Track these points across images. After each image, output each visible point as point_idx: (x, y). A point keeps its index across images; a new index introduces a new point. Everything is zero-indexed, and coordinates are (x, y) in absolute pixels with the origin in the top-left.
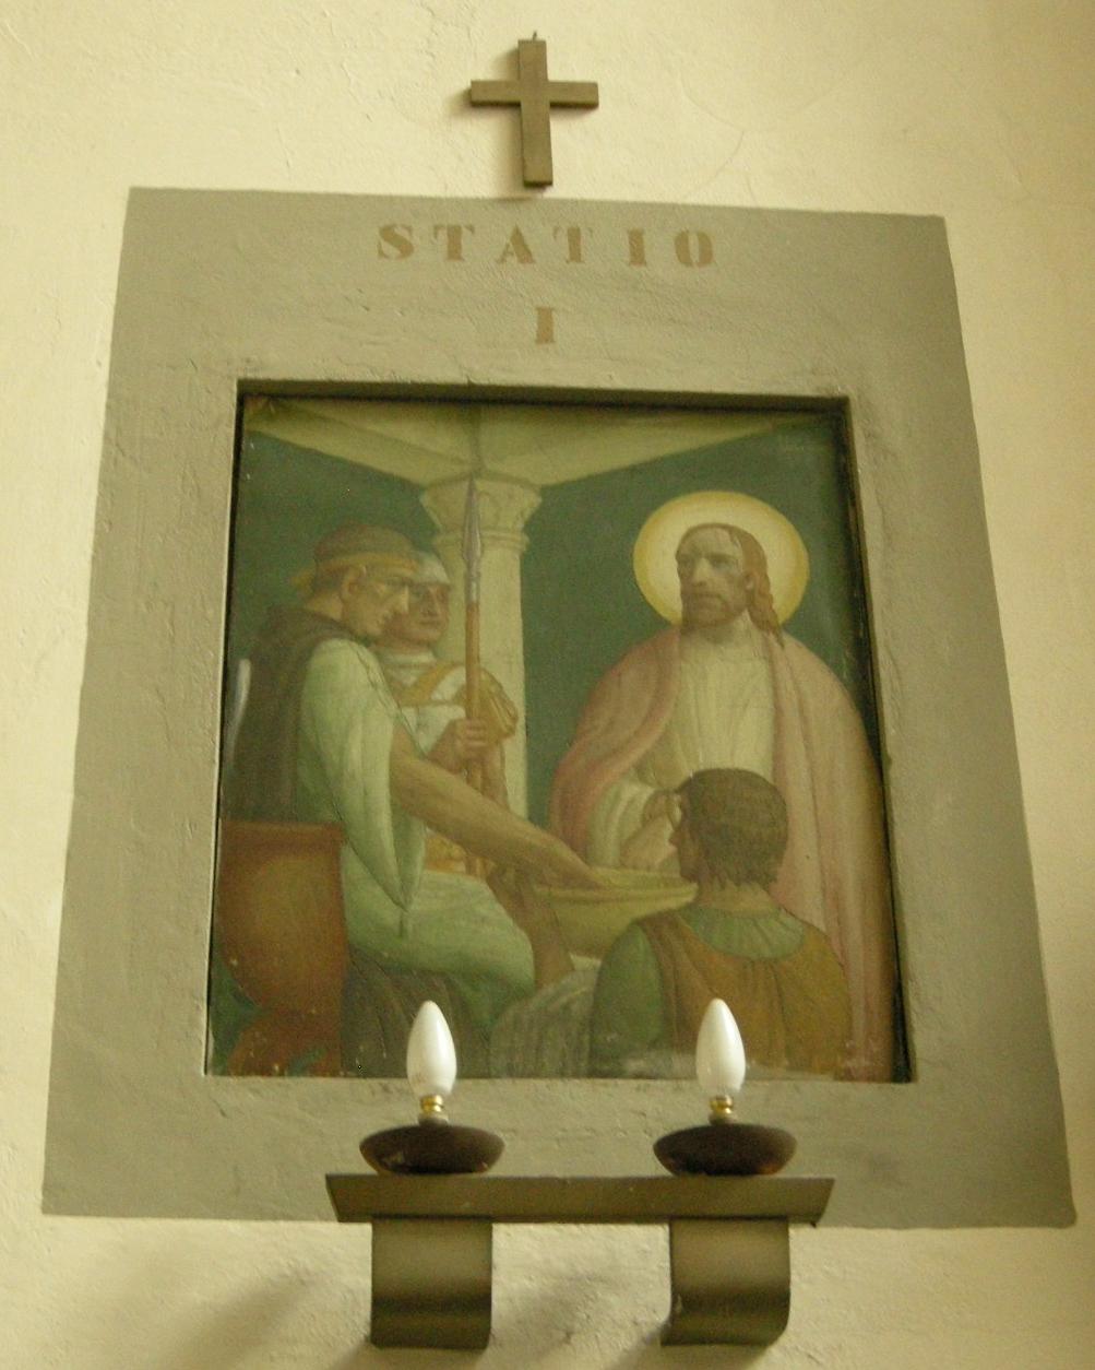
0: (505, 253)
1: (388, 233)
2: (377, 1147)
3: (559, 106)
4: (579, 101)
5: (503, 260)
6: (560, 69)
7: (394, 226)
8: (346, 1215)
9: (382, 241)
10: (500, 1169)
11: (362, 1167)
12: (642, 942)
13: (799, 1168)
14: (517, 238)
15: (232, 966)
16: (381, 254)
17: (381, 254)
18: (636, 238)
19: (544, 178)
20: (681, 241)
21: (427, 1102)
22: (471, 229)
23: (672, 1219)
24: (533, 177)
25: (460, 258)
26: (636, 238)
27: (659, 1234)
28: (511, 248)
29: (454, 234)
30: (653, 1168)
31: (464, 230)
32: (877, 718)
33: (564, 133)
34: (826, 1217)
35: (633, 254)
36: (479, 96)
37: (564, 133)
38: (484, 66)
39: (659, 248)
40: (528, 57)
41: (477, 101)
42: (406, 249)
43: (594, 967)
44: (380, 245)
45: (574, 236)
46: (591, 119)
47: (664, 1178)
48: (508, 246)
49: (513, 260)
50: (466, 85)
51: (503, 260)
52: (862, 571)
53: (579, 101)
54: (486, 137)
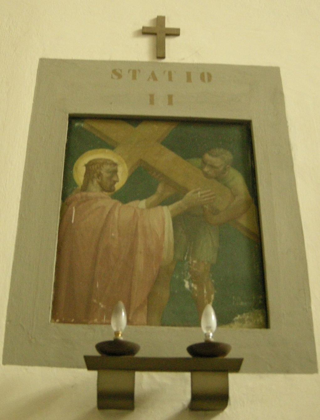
1: (114, 71)
2: (101, 347)
4: (175, 33)
5: (148, 80)
6: (169, 24)
8: (90, 368)
10: (139, 355)
11: (96, 353)
13: (231, 355)
14: (153, 74)
16: (121, 71)
17: (112, 78)
18: (189, 75)
20: (202, 75)
21: (117, 333)
22: (139, 71)
23: (192, 371)
24: (160, 56)
26: (189, 75)
27: (188, 375)
28: (151, 77)
29: (170, 74)
30: (187, 355)
32: (257, 191)
33: (170, 42)
36: (145, 31)
37: (170, 42)
38: (146, 21)
39: (195, 77)
40: (160, 20)
41: (145, 32)
42: (120, 76)
43: (210, 154)
45: (170, 74)
46: (177, 39)
49: (152, 80)
50: (141, 28)
51: (148, 80)
52: (256, 188)
53: (175, 33)
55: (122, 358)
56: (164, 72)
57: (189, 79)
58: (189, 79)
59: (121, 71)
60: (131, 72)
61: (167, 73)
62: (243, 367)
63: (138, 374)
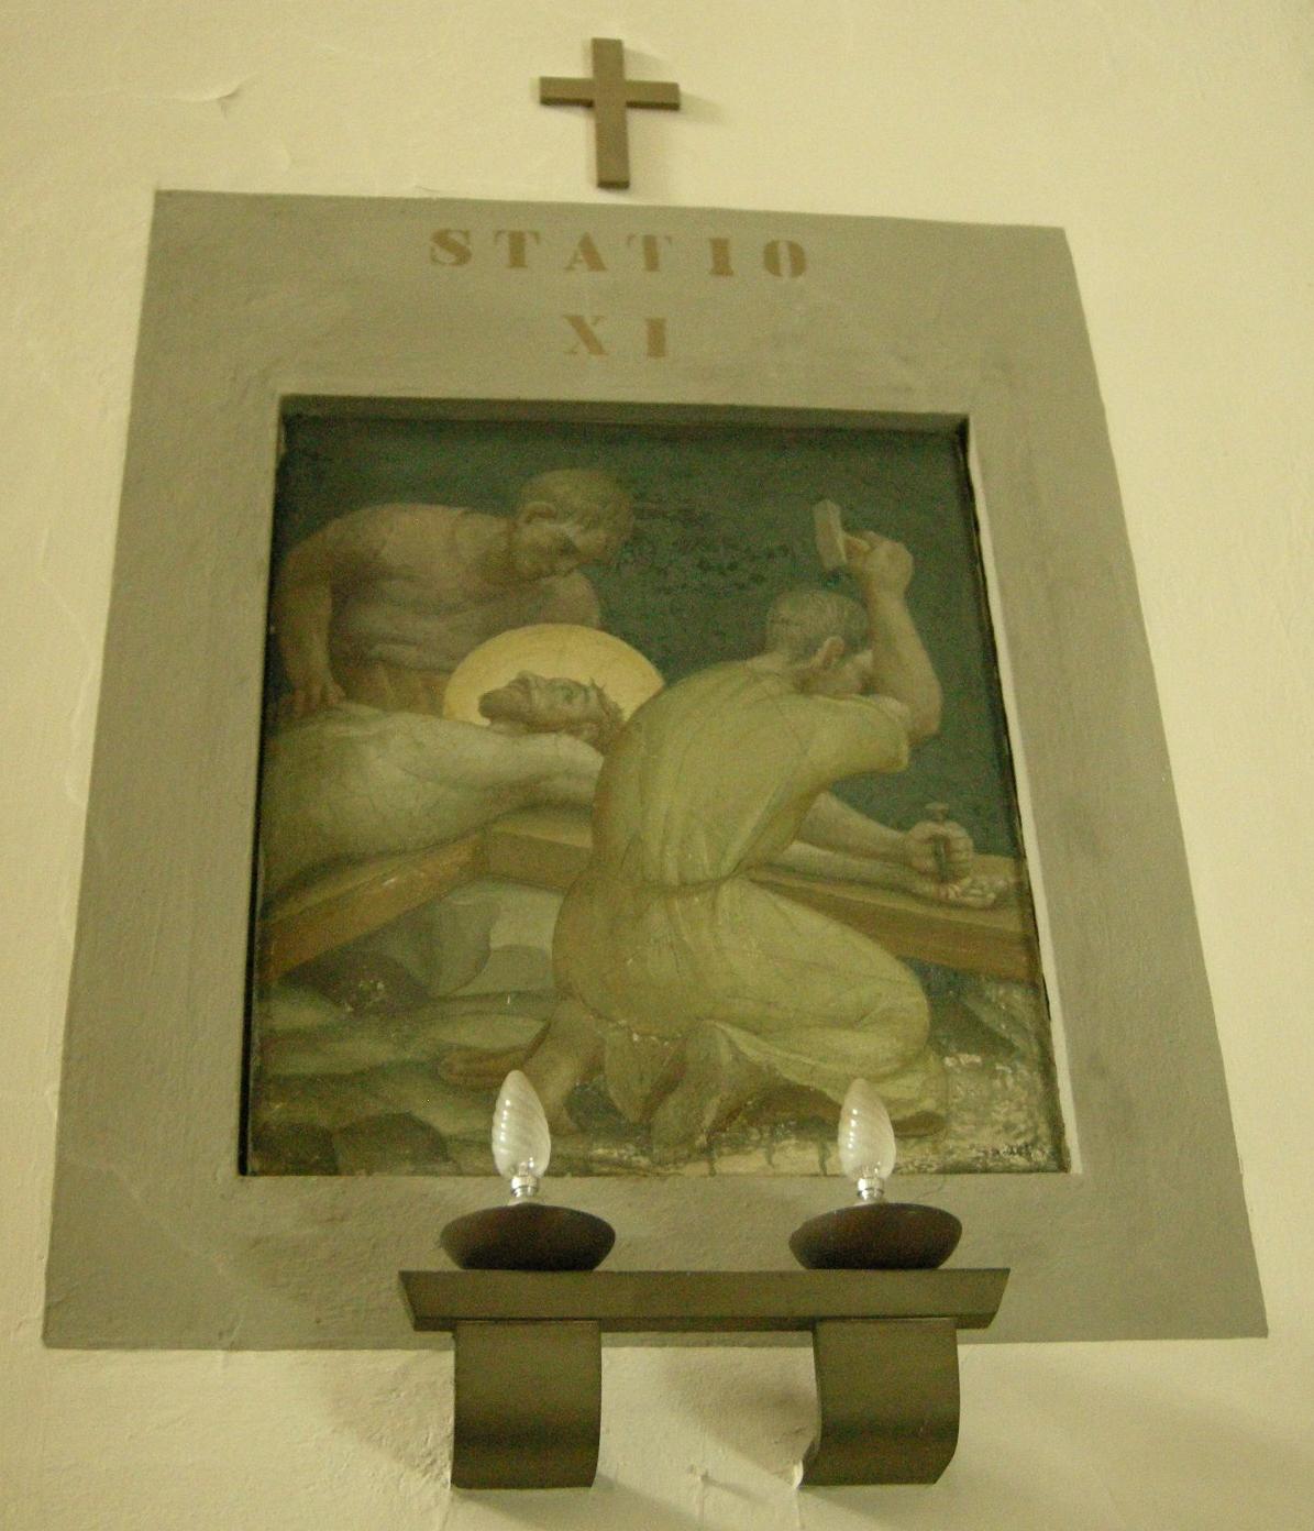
0: (575, 260)
1: (442, 239)
3: (633, 105)
4: (665, 100)
6: (652, 60)
7: (778, 242)
9: (438, 250)
11: (442, 1262)
12: (294, 1013)
15: (631, 1040)
17: (434, 260)
18: (720, 248)
19: (673, 101)
25: (729, 273)
26: (720, 248)
27: (603, 1350)
28: (581, 257)
29: (650, 243)
30: (789, 1262)
31: (527, 236)
34: (840, 1102)
35: (717, 263)
36: (551, 94)
38: (575, 67)
39: (747, 259)
40: (607, 54)
41: (555, 95)
42: (463, 256)
44: (433, 250)
45: (650, 243)
47: (452, 1275)
48: (576, 255)
53: (665, 100)
54: (575, 128)
55: (443, 1337)
56: (631, 238)
57: (722, 267)
58: (722, 267)
59: (466, 234)
60: (505, 241)
61: (638, 246)
62: (1013, 1301)
63: (812, 1350)
